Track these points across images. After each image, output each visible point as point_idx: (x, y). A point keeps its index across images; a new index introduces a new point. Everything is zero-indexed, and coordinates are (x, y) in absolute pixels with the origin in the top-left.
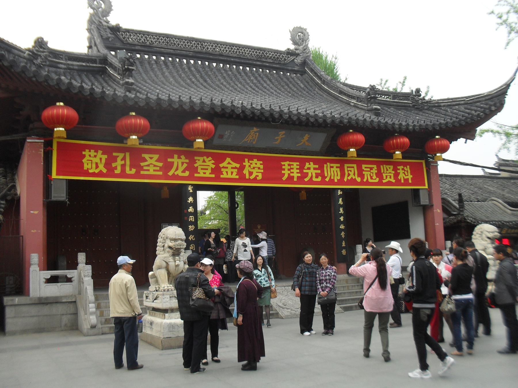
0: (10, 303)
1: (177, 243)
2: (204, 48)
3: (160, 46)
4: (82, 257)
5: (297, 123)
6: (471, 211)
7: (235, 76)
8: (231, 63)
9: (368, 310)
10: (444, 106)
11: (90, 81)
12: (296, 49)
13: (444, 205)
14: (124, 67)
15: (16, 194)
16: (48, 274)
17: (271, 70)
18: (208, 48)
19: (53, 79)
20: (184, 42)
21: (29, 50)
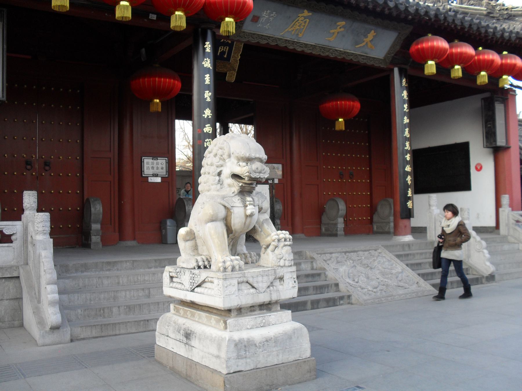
4: (30, 199)
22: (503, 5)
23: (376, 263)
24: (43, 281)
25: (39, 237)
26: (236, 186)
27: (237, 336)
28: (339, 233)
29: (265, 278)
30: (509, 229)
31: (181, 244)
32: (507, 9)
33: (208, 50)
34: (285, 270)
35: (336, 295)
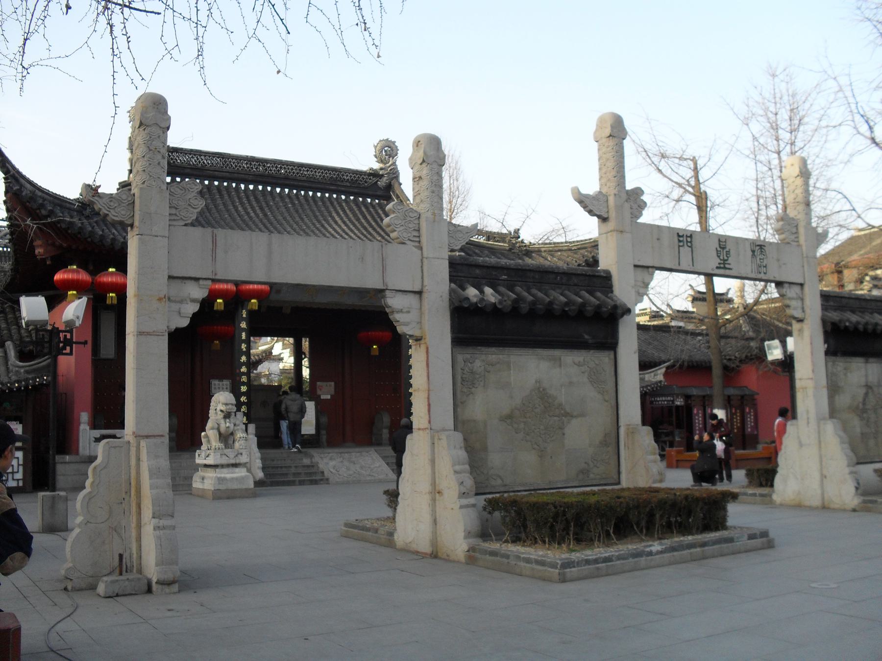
0: (61, 460)
7: (301, 205)
9: (292, 420)
12: (381, 169)
16: (97, 433)
21: (77, 200)
26: (222, 415)
27: (219, 476)
31: (203, 440)
33: (244, 316)
35: (318, 478)
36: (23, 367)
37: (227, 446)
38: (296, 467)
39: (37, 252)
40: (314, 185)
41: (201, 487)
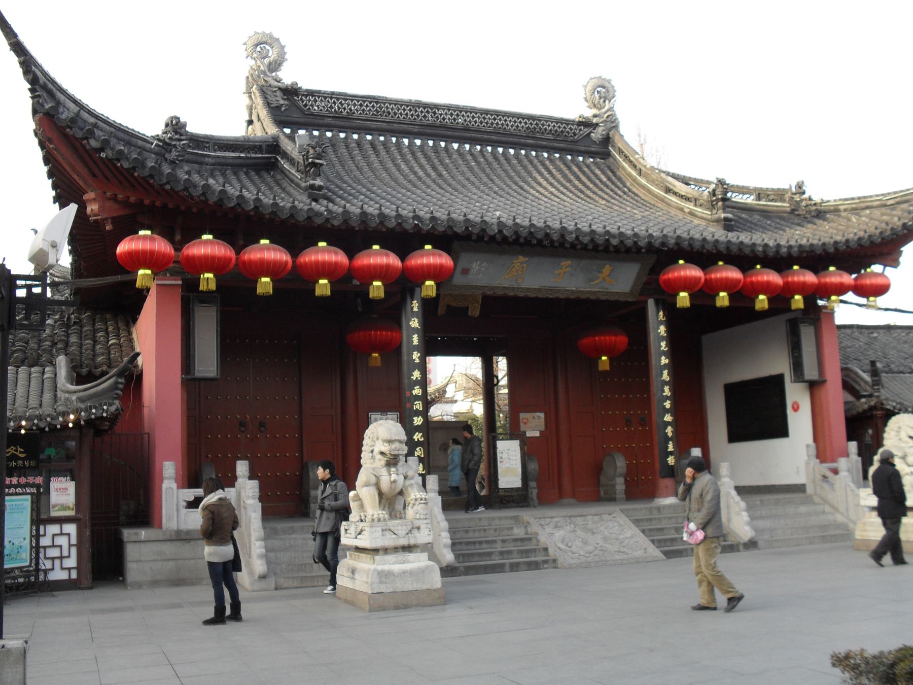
0: (134, 538)
1: (393, 446)
2: (437, 118)
3: (363, 117)
4: (242, 468)
5: (590, 247)
6: (892, 390)
7: (489, 164)
8: (484, 142)
10: (845, 210)
11: (254, 184)
12: (595, 116)
13: (846, 379)
14: (308, 159)
15: (136, 366)
17: (551, 152)
18: (444, 119)
19: (195, 186)
20: (404, 110)
21: (157, 138)
22: (810, 199)
23: (602, 528)
24: (253, 539)
25: (250, 502)
26: (382, 461)
27: (380, 568)
28: (618, 496)
29: (404, 527)
30: (815, 488)
31: (353, 505)
32: (815, 204)
33: (415, 309)
34: (421, 521)
35: (540, 558)
36: (75, 392)
37: (393, 515)
38: (503, 541)
39: (89, 210)
40: (503, 139)
41: (350, 585)
